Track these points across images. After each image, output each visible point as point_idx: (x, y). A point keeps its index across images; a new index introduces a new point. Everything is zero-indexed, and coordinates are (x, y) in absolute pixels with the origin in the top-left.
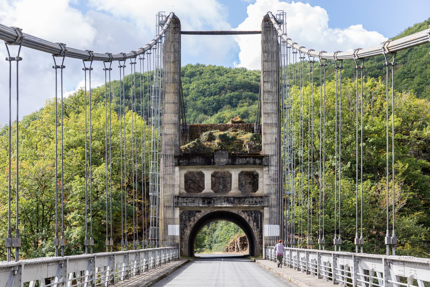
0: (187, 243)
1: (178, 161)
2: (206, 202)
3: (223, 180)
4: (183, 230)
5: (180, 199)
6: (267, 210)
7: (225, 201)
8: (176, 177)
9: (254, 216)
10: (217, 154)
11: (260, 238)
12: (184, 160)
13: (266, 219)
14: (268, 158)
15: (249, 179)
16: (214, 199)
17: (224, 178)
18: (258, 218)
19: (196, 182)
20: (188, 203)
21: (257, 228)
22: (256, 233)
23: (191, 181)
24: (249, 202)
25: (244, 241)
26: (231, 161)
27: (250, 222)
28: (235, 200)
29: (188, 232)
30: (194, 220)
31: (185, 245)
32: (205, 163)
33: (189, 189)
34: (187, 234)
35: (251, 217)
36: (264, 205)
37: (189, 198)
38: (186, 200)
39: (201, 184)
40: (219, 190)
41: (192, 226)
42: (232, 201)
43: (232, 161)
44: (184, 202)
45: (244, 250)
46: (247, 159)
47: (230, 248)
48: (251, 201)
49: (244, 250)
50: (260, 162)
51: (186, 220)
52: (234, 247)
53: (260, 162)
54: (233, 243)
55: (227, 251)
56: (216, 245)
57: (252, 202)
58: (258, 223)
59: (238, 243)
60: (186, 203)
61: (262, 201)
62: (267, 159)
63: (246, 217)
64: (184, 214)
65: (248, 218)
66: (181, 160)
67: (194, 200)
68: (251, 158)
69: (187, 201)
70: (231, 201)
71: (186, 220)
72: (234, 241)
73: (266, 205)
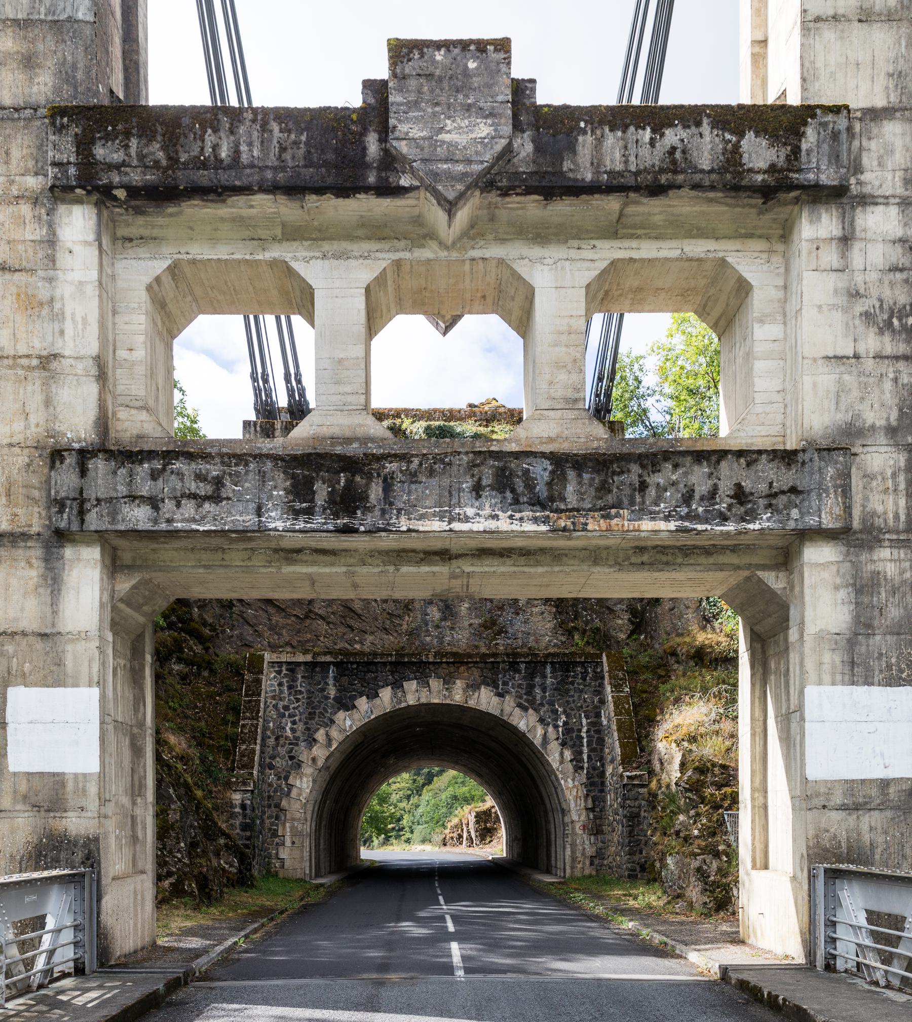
0: (307, 828)
1: (84, 145)
2: (322, 492)
4: (286, 778)
5: (99, 466)
6: (824, 566)
7: (477, 490)
8: (65, 289)
9: (565, 723)
10: (413, 83)
11: (587, 809)
12: (134, 143)
13: (820, 637)
14: (842, 123)
16: (391, 467)
18: (580, 731)
20: (169, 505)
21: (576, 771)
22: (571, 790)
24: (687, 498)
25: (486, 822)
26: (529, 147)
27: (549, 747)
28: (564, 479)
29: (305, 785)
30: (329, 740)
31: (292, 836)
32: (309, 164)
34: (300, 795)
35: (551, 729)
36: (812, 521)
37: (177, 465)
38: (154, 475)
40: (427, 625)
41: (320, 763)
42: (541, 489)
43: (539, 149)
44: (133, 498)
45: (487, 842)
46: (672, 137)
47: (452, 838)
48: (702, 488)
50: (781, 162)
52: (460, 836)
53: (781, 162)
54: (459, 826)
55: (445, 845)
56: (420, 827)
57: (713, 493)
58: (581, 753)
59: (471, 826)
60: (154, 502)
61: (793, 490)
62: (835, 136)
63: (535, 727)
65: (540, 731)
66: (107, 137)
67: (218, 482)
68: (706, 128)
69: (167, 486)
70: (530, 484)
71: (297, 739)
73: (828, 522)
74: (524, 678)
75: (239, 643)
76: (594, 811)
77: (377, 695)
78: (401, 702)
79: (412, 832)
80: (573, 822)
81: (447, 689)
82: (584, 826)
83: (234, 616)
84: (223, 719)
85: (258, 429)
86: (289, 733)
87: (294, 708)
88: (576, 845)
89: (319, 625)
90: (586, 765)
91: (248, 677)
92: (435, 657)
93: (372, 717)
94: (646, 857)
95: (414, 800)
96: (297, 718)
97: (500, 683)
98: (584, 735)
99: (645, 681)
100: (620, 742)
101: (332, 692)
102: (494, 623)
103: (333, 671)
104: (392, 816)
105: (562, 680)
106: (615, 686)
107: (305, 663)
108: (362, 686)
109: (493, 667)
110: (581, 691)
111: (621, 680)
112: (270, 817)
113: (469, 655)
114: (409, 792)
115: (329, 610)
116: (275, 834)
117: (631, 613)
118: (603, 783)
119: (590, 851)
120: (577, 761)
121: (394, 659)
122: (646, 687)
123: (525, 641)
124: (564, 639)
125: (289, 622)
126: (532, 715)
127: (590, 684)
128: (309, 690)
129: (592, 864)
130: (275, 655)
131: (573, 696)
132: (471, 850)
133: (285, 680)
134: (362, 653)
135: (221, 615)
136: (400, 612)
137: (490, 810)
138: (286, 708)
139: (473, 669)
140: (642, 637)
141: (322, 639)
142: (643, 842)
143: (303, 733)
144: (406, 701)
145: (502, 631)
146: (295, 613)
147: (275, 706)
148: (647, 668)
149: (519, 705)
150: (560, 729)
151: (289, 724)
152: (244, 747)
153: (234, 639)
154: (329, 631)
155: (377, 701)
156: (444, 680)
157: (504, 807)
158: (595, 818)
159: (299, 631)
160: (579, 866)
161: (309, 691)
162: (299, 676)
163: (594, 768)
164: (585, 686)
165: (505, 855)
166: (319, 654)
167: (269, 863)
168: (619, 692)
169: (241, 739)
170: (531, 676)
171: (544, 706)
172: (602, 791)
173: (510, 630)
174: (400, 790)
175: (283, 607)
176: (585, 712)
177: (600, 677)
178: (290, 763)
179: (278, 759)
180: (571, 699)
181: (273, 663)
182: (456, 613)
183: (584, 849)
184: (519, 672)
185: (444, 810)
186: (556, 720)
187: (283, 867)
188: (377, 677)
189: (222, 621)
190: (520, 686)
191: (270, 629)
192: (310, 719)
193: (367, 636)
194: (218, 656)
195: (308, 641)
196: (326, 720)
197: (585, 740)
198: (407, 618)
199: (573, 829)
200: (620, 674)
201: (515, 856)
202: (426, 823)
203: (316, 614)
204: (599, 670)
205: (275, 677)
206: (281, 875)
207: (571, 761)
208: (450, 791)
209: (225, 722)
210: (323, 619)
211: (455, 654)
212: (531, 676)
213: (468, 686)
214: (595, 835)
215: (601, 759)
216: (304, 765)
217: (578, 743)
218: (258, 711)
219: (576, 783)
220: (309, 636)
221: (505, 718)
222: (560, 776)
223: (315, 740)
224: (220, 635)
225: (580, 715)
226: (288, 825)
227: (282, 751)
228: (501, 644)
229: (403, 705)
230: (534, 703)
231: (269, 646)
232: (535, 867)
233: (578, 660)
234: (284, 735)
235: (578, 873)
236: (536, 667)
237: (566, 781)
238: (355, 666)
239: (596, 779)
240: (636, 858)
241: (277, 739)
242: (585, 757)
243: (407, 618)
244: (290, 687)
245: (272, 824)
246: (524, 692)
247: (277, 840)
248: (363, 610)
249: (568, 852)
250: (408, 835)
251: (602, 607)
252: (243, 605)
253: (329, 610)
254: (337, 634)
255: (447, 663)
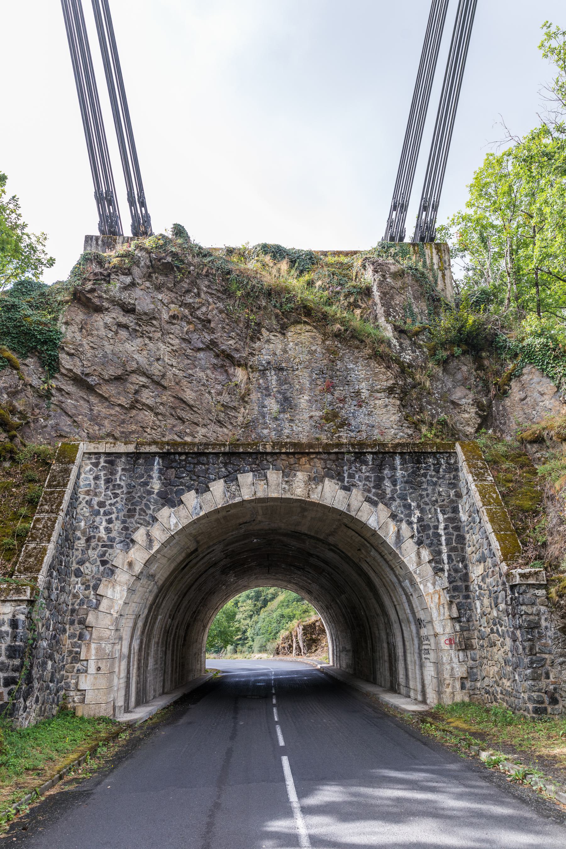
3: (279, 380)
4: (96, 587)
9: (420, 520)
11: (452, 619)
15: (384, 374)
17: (282, 369)
18: (436, 527)
19: (165, 384)
23: (143, 380)
25: (312, 634)
27: (404, 546)
29: (117, 596)
30: (150, 540)
33: (134, 412)
34: (111, 607)
35: (404, 525)
39: (188, 392)
40: (264, 417)
41: (138, 568)
45: (313, 651)
47: (284, 648)
49: (311, 653)
51: (112, 540)
52: (291, 646)
54: (289, 638)
55: (278, 654)
56: (259, 637)
58: (440, 553)
63: (386, 523)
64: (105, 514)
71: (112, 540)
72: (291, 633)
74: (372, 470)
75: (54, 434)
76: (460, 622)
77: (207, 489)
78: (234, 496)
79: (253, 641)
80: (436, 635)
81: (287, 482)
82: (450, 640)
83: (52, 406)
84: (15, 513)
85: (100, 242)
86: (103, 533)
87: (111, 505)
88: (443, 664)
89: (146, 416)
90: (446, 567)
91: (55, 467)
92: (273, 447)
93: (202, 514)
94: (554, 683)
95: (255, 618)
96: (113, 516)
97: (346, 475)
98: (441, 532)
99: (507, 471)
100: (496, 535)
101: (156, 485)
102: (335, 415)
103: (158, 463)
104: (238, 630)
105: (413, 472)
106: (477, 475)
107: (127, 454)
108: (191, 479)
109: (337, 459)
110: (435, 484)
111: (481, 468)
112: (72, 636)
113: (310, 446)
114: (251, 613)
115: (158, 400)
116: (76, 658)
117: (478, 407)
118: (467, 588)
119: (460, 671)
120: (437, 562)
121: (227, 450)
122: (509, 476)
123: (369, 433)
124: (410, 432)
125: (113, 412)
126: (383, 511)
127: (444, 476)
128: (130, 485)
129: (463, 687)
130: (93, 445)
131: (426, 489)
132: (299, 659)
133: (102, 473)
134: (193, 444)
135: (37, 405)
136: (236, 404)
137: (314, 624)
138: (101, 504)
139: (316, 460)
140: (490, 431)
141: (148, 430)
142: (548, 662)
143: (119, 533)
144: (240, 496)
145: (344, 424)
146: (119, 402)
147: (89, 503)
148: (507, 457)
149: (368, 500)
150: (415, 526)
151: (104, 524)
152: (32, 545)
153: (48, 429)
154: (157, 422)
155: (207, 496)
156: (283, 472)
157: (333, 620)
158: (462, 629)
159: (123, 422)
160: (449, 690)
161: (129, 486)
162: (119, 469)
163: (456, 571)
164: (439, 478)
165: (331, 664)
166: (142, 444)
167: (65, 697)
168: (481, 480)
169: (31, 536)
170: (380, 468)
171: (395, 500)
172: (467, 597)
173: (353, 423)
174: (245, 611)
175: (107, 396)
176: (441, 507)
177: (454, 469)
178: (102, 568)
179: (87, 564)
180: (424, 493)
181: (90, 454)
182: (296, 405)
183: (452, 669)
184: (365, 463)
185: (275, 625)
186: (409, 515)
187: (83, 701)
188: (208, 469)
189: (37, 411)
190: (367, 478)
191: (91, 420)
192: (129, 517)
193: (198, 428)
194: (25, 446)
195: (133, 432)
196: (147, 518)
197: (443, 538)
198: (242, 410)
199: (437, 644)
200: (480, 464)
201: (344, 666)
202: (263, 634)
203: (144, 404)
204: (452, 461)
205: (91, 470)
206: (79, 713)
207: (430, 562)
208: (279, 612)
209: (16, 516)
210: (151, 408)
211: (294, 445)
212: (380, 468)
213: (310, 479)
214: (463, 650)
215: (463, 559)
216: (117, 571)
217: (435, 541)
218: (60, 503)
219: (438, 588)
220: (134, 427)
221: (353, 514)
222: (418, 580)
223: (133, 541)
224: (32, 425)
225: (435, 510)
226: (93, 646)
227: (93, 554)
228: (344, 436)
229: (237, 500)
230: (384, 498)
231: (88, 437)
232: (373, 680)
233: (429, 450)
234: (97, 535)
235: (447, 701)
236: (384, 458)
237: (425, 586)
238: (183, 457)
239: (459, 583)
240: (543, 683)
241: (88, 540)
242: (445, 557)
243: (242, 410)
244: (108, 481)
245: (74, 645)
246: (372, 485)
247: (78, 666)
248: (195, 401)
249: (430, 671)
250: (251, 643)
251: (446, 402)
252: (62, 395)
253: (158, 400)
254: (165, 425)
255: (287, 454)
